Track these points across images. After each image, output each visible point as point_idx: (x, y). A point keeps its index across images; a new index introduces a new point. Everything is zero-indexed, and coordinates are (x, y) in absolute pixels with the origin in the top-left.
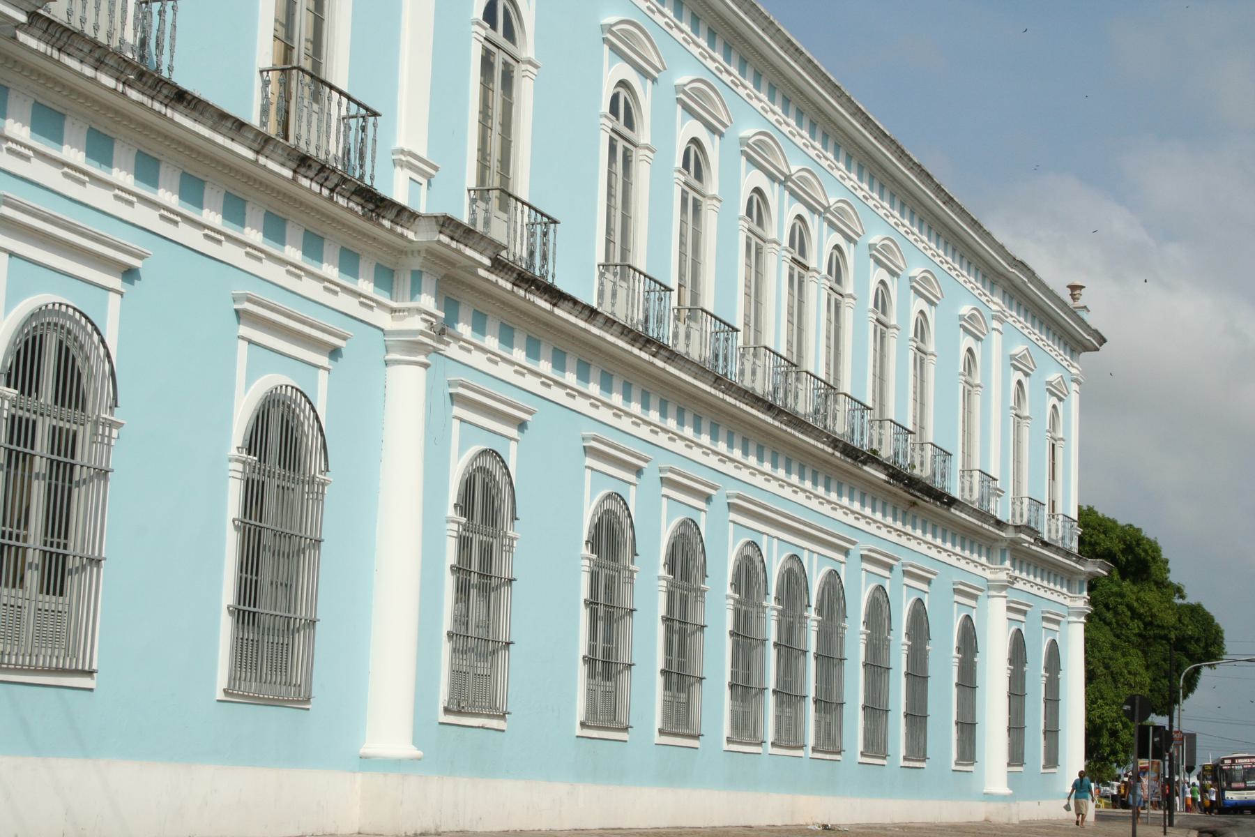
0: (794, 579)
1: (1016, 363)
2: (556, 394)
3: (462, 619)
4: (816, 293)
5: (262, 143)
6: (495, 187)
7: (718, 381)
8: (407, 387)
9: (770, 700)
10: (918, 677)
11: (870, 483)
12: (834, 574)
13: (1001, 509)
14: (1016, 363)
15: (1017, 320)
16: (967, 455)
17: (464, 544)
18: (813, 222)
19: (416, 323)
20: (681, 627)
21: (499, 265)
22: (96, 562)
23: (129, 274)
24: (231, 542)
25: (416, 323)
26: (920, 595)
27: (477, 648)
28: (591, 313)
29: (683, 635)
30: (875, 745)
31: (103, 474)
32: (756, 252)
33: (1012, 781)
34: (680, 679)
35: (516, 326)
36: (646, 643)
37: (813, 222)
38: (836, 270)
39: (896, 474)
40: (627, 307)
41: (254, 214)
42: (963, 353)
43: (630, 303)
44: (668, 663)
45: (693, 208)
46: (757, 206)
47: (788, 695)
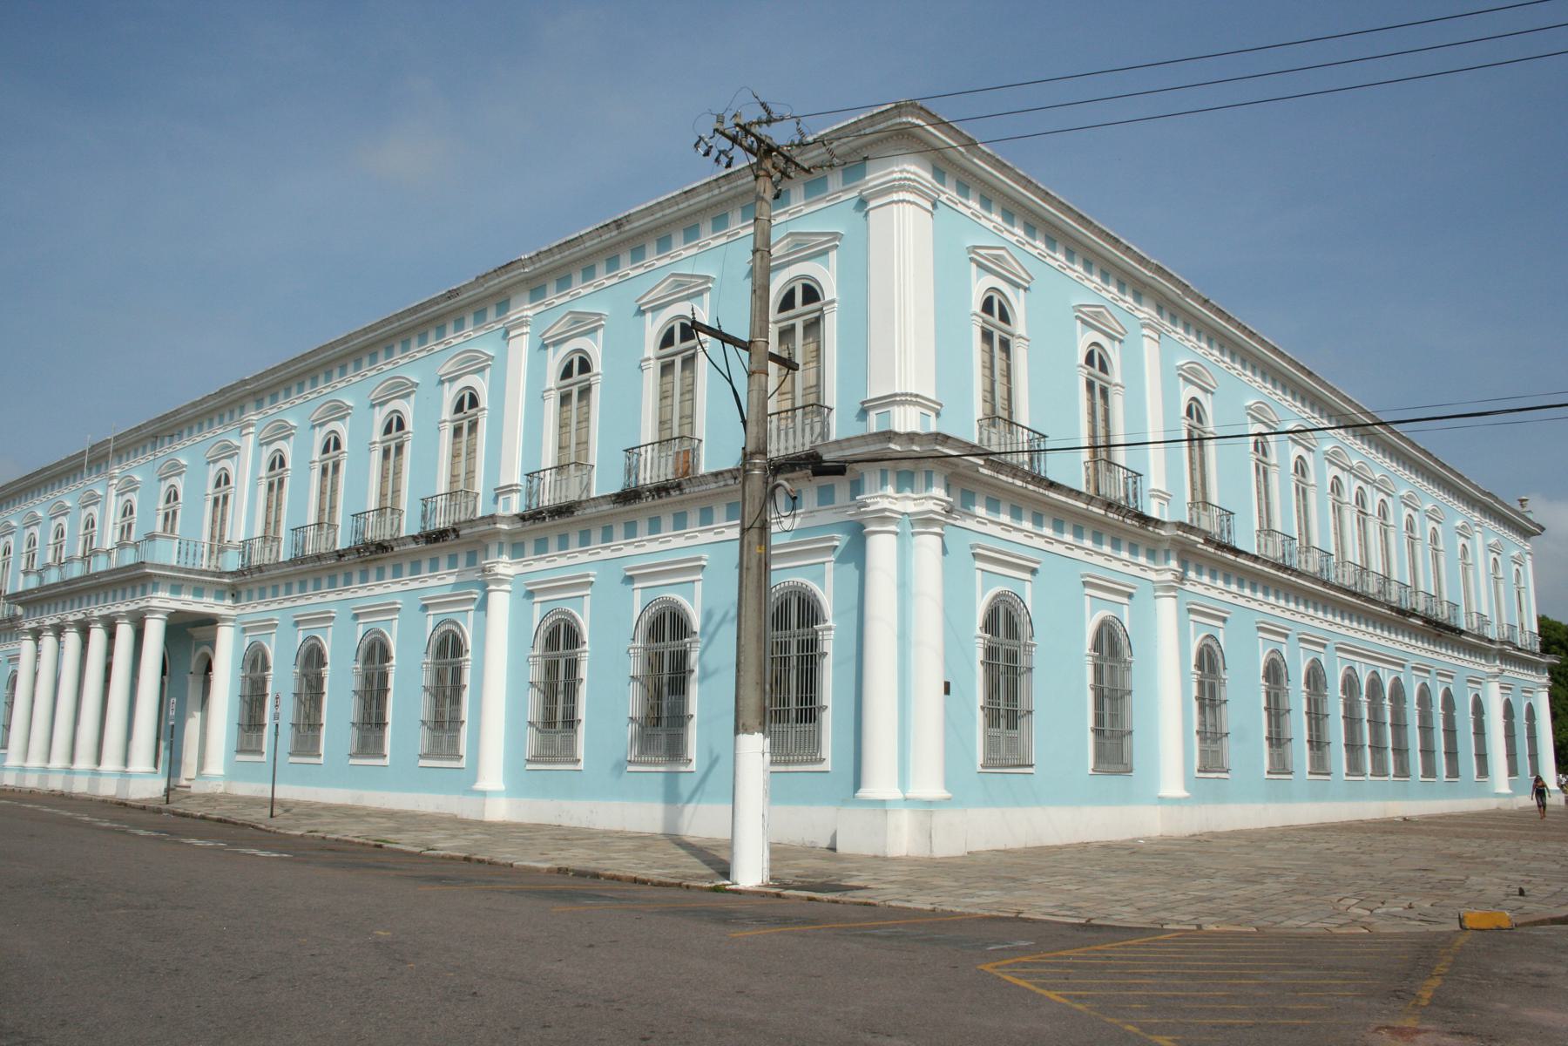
0: (1375, 684)
1: (1491, 548)
2: (1241, 601)
3: (1203, 723)
4: (1373, 527)
5: (1090, 500)
6: (1201, 501)
7: (1325, 583)
8: (1167, 608)
9: (1368, 751)
10: (1450, 731)
11: (1414, 626)
12: (1397, 679)
13: (1491, 632)
14: (1491, 548)
15: (1489, 524)
16: (1468, 604)
17: (1201, 684)
18: (1368, 489)
19: (1169, 576)
20: (1316, 716)
21: (1208, 541)
22: (1030, 712)
23: (1034, 571)
24: (1090, 696)
25: (1169, 576)
26: (1277, 646)
27: (1211, 736)
28: (1256, 558)
29: (1317, 719)
30: (1429, 770)
31: (1030, 669)
32: (1338, 510)
33: (1512, 785)
34: (1318, 743)
35: (1220, 569)
36: (1298, 726)
37: (1368, 489)
38: (1383, 513)
39: (1428, 620)
40: (1274, 551)
41: (1087, 533)
42: (1460, 548)
43: (1275, 549)
44: (1270, 732)
45: (1302, 493)
46: (1336, 486)
47: (1378, 748)
